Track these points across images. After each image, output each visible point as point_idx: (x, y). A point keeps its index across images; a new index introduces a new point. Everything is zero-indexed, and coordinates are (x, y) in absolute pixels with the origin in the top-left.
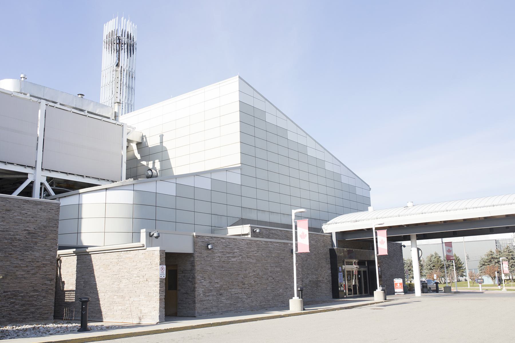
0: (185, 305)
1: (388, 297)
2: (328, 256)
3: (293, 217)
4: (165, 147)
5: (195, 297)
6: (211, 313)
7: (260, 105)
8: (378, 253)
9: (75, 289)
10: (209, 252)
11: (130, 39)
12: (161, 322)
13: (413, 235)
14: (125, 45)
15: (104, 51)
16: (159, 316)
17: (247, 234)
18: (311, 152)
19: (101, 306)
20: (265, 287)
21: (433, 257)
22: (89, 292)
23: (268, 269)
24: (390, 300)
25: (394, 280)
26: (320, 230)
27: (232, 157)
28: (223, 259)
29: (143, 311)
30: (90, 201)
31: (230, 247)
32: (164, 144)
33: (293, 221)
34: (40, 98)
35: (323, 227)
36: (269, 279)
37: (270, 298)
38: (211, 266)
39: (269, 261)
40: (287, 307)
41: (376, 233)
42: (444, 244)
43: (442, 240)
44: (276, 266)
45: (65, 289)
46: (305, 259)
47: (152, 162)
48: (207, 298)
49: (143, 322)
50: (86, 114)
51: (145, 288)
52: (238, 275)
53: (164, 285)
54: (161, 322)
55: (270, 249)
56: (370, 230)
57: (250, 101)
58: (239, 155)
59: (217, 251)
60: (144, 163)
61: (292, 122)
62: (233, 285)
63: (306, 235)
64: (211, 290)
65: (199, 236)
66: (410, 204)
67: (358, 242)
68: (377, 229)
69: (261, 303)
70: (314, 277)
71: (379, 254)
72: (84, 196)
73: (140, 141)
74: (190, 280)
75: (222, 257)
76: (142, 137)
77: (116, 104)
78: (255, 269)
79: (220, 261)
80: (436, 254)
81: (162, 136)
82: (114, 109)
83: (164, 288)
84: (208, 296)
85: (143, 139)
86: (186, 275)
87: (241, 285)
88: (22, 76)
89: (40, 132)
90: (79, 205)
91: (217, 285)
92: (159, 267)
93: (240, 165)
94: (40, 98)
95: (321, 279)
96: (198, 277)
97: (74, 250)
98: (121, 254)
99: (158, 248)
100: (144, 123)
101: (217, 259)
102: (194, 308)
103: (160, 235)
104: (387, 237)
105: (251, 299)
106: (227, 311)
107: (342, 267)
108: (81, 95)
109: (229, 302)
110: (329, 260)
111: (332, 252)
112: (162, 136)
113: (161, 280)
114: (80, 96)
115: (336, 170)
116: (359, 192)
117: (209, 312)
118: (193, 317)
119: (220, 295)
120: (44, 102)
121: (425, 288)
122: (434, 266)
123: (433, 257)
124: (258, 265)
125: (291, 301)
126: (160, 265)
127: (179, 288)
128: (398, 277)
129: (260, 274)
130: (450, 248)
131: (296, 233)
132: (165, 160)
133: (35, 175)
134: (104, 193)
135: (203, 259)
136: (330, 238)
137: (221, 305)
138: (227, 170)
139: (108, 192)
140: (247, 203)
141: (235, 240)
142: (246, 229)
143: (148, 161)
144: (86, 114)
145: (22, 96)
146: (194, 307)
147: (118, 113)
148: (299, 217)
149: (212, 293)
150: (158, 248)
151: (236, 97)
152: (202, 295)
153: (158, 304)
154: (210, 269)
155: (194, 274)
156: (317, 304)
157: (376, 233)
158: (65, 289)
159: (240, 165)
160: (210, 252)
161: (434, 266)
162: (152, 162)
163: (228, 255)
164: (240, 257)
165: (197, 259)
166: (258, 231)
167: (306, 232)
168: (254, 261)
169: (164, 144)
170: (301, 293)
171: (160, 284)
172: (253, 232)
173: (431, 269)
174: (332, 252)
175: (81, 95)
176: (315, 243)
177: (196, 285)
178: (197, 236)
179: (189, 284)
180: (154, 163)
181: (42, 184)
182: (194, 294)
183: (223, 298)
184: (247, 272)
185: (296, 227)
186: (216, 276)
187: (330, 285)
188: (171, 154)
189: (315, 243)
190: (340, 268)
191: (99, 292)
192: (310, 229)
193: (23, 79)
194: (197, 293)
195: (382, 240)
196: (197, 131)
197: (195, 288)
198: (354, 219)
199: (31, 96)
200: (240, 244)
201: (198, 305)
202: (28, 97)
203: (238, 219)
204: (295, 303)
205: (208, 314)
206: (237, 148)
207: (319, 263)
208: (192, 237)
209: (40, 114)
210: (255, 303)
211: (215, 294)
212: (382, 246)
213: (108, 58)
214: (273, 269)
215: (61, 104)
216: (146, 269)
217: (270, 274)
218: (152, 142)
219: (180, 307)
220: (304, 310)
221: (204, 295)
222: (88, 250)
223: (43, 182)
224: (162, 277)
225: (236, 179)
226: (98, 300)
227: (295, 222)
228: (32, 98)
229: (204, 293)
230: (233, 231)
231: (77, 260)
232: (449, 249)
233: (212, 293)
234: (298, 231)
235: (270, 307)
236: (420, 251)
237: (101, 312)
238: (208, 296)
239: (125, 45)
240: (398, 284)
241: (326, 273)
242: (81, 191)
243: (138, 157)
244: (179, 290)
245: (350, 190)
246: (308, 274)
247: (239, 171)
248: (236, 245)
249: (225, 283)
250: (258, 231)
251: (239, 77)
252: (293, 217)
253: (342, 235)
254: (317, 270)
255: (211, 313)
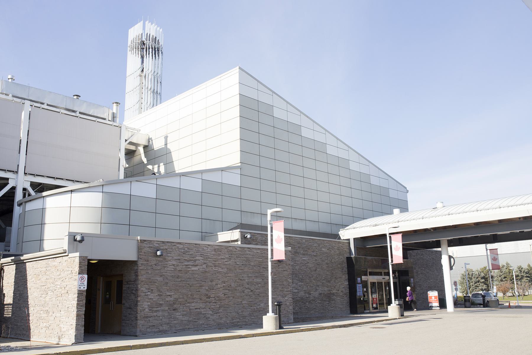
0: (127, 322)
1: (406, 314)
2: (345, 265)
3: (269, 218)
4: (169, 150)
5: (137, 313)
6: (160, 331)
7: (265, 98)
8: (392, 261)
9: (12, 303)
10: (159, 259)
11: (155, 43)
12: (77, 342)
13: (444, 240)
14: (149, 48)
15: (129, 53)
16: (75, 336)
17: (237, 241)
18: (330, 150)
19: (31, 322)
20: (240, 300)
21: (505, 268)
22: (22, 306)
23: (244, 280)
24: (408, 317)
25: (428, 293)
26: (337, 236)
27: (234, 158)
28: (179, 268)
29: (63, 330)
30: (54, 205)
31: (190, 253)
32: (169, 146)
33: (269, 223)
34: (24, 99)
35: (339, 233)
36: (246, 291)
37: (246, 314)
38: (161, 276)
39: (245, 270)
40: (261, 326)
41: (390, 237)
42: (488, 251)
43: (486, 247)
44: (256, 277)
45: (5, 303)
46: (314, 268)
47: (157, 166)
48: (155, 314)
49: (62, 343)
50: (78, 114)
51: (65, 302)
52: (201, 286)
53: (84, 298)
54: (77, 342)
55: (247, 256)
56: (383, 237)
57: (253, 94)
58: (238, 154)
59: (170, 258)
60: (150, 167)
61: (308, 117)
62: (194, 299)
63: (282, 239)
64: (161, 305)
65: (145, 241)
66: (439, 205)
67: (373, 248)
68: (390, 234)
69: (233, 320)
70: (326, 289)
71: (394, 262)
72: (48, 199)
73: (147, 144)
74: (134, 292)
75: (178, 265)
76: (149, 140)
77: (115, 104)
78: (226, 280)
79: (175, 269)
80: (508, 264)
81: (166, 138)
82: (112, 109)
83: (84, 302)
84: (156, 311)
85: (149, 142)
86: (130, 286)
87: (204, 298)
88: (10, 77)
89: (23, 135)
90: (43, 210)
91: (168, 299)
92: (77, 277)
93: (240, 164)
94: (24, 99)
95: (334, 291)
96: (143, 288)
97: (13, 258)
98: (49, 262)
99: (77, 254)
100: (144, 124)
101: (171, 268)
102: (135, 326)
103: (85, 238)
104: (403, 245)
105: (218, 314)
106: (183, 330)
107: (361, 279)
108: (76, 95)
109: (186, 318)
110: (346, 269)
111: (349, 259)
112: (166, 138)
113: (80, 293)
114: (75, 97)
115: (364, 170)
116: (393, 194)
117: (157, 330)
118: (135, 336)
119: (174, 310)
120: (28, 103)
121: (457, 303)
122: (505, 278)
123: (505, 268)
124: (229, 275)
125: (264, 317)
126: (79, 274)
127: (123, 302)
128: (432, 289)
129: (233, 285)
130: (496, 256)
131: (272, 236)
132: (169, 163)
133: (16, 180)
134: (69, 195)
135: (149, 268)
136: (347, 245)
137: (175, 322)
138: (222, 170)
139: (74, 195)
140: (247, 206)
141: (227, 246)
142: (236, 235)
143: (153, 165)
144: (78, 114)
145: (4, 97)
146: (136, 324)
147: (117, 114)
148: (276, 217)
149: (162, 308)
150: (77, 254)
151: (235, 90)
152: (147, 310)
153: (75, 321)
154: (161, 279)
155: (137, 285)
156: (299, 322)
157: (390, 237)
158: (5, 303)
159: (240, 164)
160: (161, 259)
161: (505, 278)
162: (157, 166)
163: (186, 263)
164: (204, 266)
165: (141, 268)
166: (249, 236)
167: (282, 235)
168: (225, 270)
169: (168, 146)
170: (278, 308)
171: (78, 297)
172: (244, 238)
173: (502, 281)
174: (349, 259)
175: (76, 95)
176: (328, 251)
177: (139, 299)
178: (142, 241)
179: (133, 297)
180: (159, 167)
181: (24, 189)
182: (137, 309)
183: (178, 314)
184: (214, 283)
185: (272, 228)
186: (168, 288)
187: (346, 299)
188: (175, 156)
189: (328, 251)
190: (359, 279)
191: (30, 306)
192: (286, 231)
193: (10, 80)
194: (139, 308)
195: (397, 246)
196: (197, 130)
197: (137, 301)
198: (374, 224)
199: (14, 96)
200: (203, 250)
201: (140, 322)
202: (10, 97)
203: (236, 225)
204: (269, 321)
205: (155, 332)
206: (237, 146)
207: (333, 273)
208: (136, 241)
209: (24, 116)
210: (224, 319)
211: (167, 308)
212: (397, 255)
213: (133, 61)
214: (251, 280)
215: (48, 105)
216: (67, 279)
217: (247, 286)
218: (157, 145)
219: (124, 324)
220: (281, 328)
221: (150, 310)
222: (22, 258)
223: (26, 187)
224: (82, 288)
225: (235, 179)
226: (28, 315)
227: (270, 224)
228: (15, 99)
229: (151, 308)
230: (224, 237)
231: (16, 269)
232: (494, 257)
233: (162, 308)
234: (274, 234)
235: (246, 325)
236: (452, 259)
237: (30, 329)
238: (156, 311)
239: (149, 48)
240: (433, 298)
241: (343, 284)
242: (45, 194)
243: (145, 160)
244: (124, 304)
245: (383, 192)
246: (318, 286)
247: (238, 171)
248: (198, 251)
249: (181, 297)
250: (249, 236)
251: (240, 68)
252: (269, 218)
253: (362, 242)
254: (329, 282)
255: (160, 331)
